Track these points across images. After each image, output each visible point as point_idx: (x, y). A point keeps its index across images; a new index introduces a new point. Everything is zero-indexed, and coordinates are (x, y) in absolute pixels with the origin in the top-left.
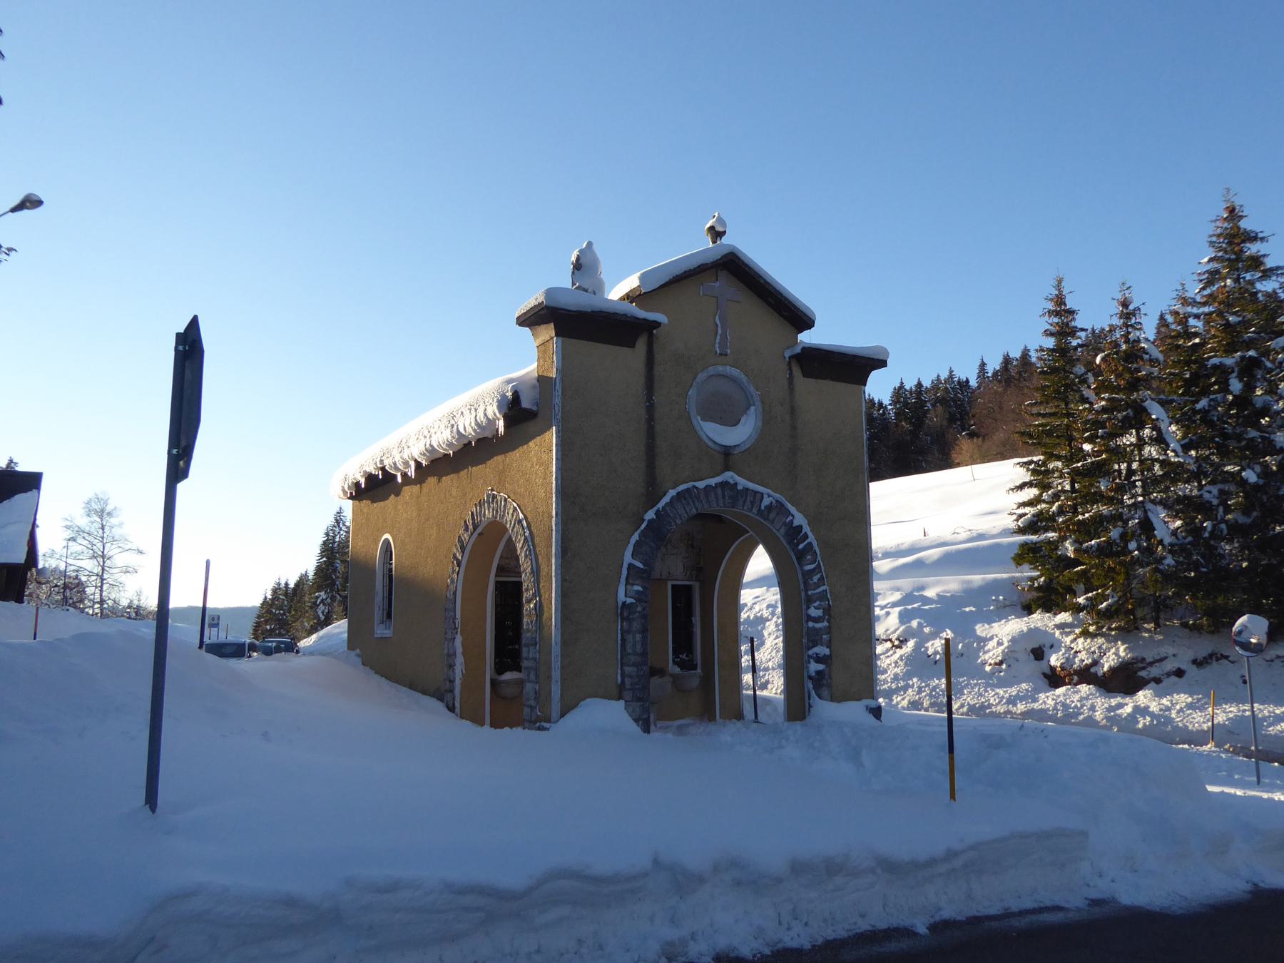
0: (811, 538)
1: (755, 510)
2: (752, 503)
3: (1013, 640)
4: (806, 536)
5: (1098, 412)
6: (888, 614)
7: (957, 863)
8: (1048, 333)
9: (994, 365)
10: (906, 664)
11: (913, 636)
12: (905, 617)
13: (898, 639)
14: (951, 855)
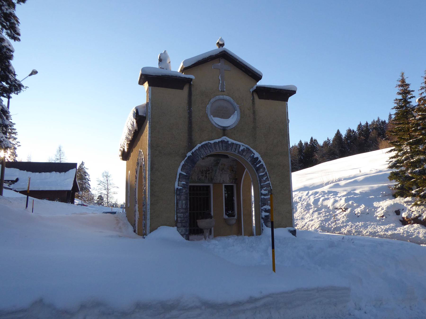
0: (262, 162)
1: (237, 152)
2: (235, 149)
3: (388, 208)
4: (260, 161)
5: (418, 120)
6: (341, 199)
7: (258, 304)
8: (400, 94)
10: (347, 217)
11: (350, 207)
12: (347, 201)
13: (344, 208)
14: (252, 300)
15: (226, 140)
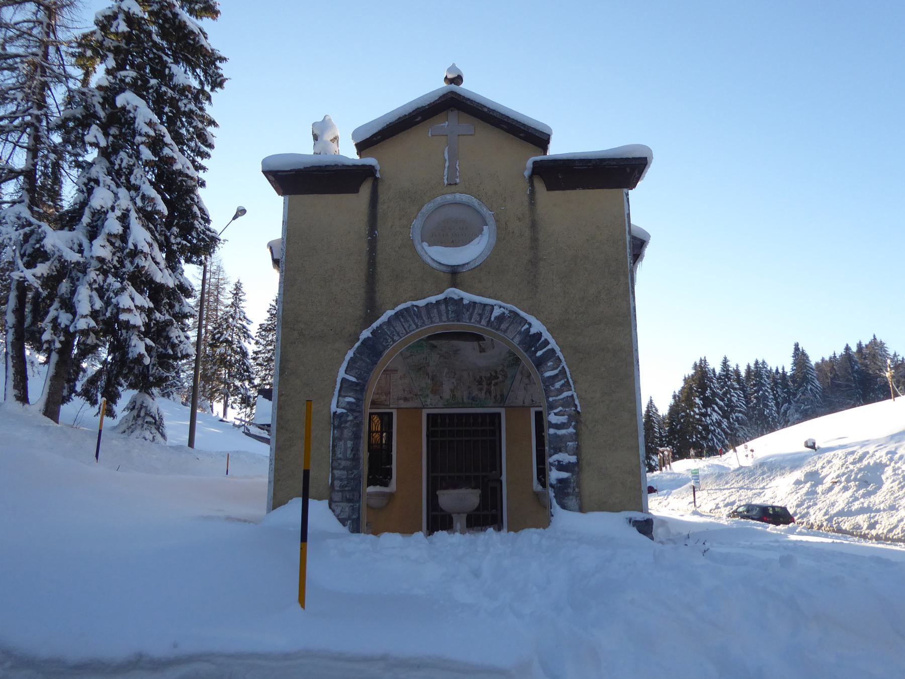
1: (484, 322)
2: (481, 316)
15: (456, 297)
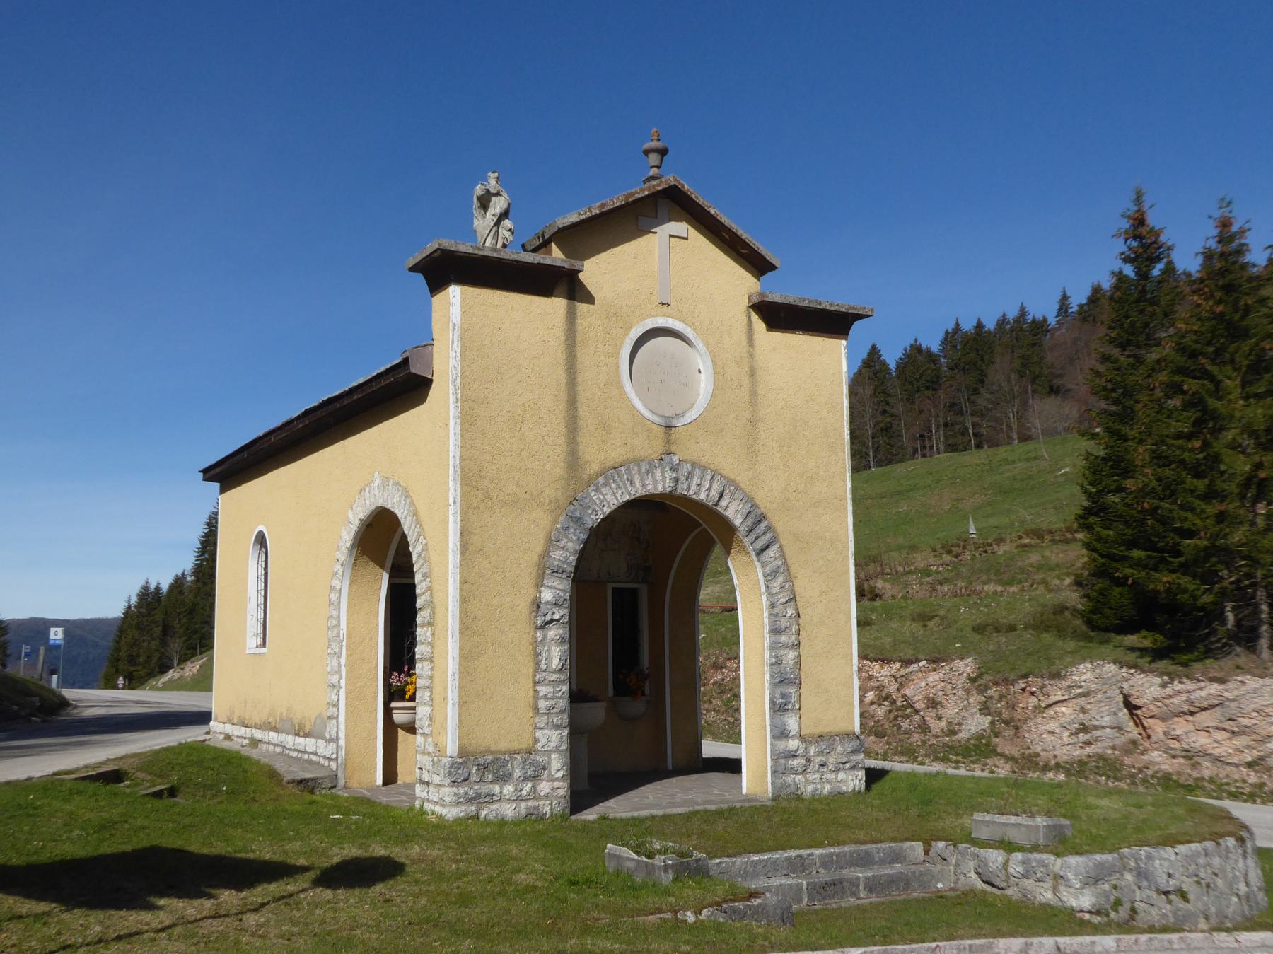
9: (1079, 297)
